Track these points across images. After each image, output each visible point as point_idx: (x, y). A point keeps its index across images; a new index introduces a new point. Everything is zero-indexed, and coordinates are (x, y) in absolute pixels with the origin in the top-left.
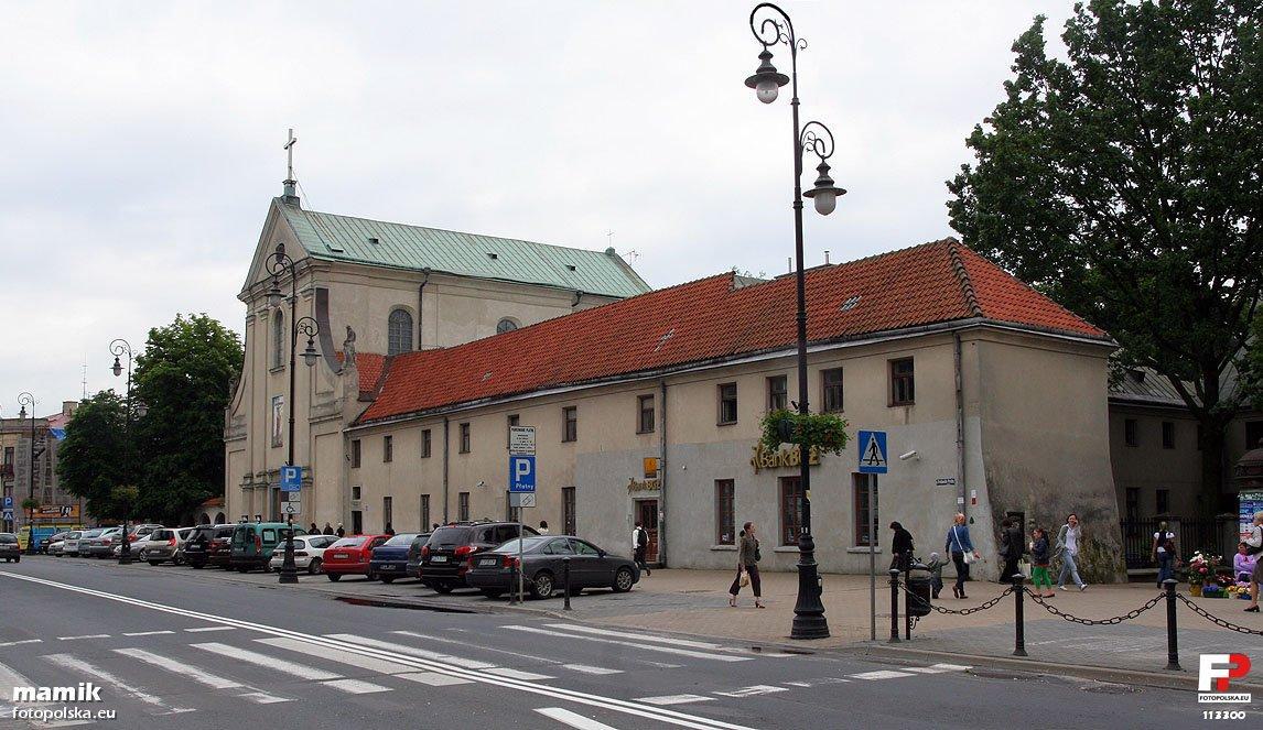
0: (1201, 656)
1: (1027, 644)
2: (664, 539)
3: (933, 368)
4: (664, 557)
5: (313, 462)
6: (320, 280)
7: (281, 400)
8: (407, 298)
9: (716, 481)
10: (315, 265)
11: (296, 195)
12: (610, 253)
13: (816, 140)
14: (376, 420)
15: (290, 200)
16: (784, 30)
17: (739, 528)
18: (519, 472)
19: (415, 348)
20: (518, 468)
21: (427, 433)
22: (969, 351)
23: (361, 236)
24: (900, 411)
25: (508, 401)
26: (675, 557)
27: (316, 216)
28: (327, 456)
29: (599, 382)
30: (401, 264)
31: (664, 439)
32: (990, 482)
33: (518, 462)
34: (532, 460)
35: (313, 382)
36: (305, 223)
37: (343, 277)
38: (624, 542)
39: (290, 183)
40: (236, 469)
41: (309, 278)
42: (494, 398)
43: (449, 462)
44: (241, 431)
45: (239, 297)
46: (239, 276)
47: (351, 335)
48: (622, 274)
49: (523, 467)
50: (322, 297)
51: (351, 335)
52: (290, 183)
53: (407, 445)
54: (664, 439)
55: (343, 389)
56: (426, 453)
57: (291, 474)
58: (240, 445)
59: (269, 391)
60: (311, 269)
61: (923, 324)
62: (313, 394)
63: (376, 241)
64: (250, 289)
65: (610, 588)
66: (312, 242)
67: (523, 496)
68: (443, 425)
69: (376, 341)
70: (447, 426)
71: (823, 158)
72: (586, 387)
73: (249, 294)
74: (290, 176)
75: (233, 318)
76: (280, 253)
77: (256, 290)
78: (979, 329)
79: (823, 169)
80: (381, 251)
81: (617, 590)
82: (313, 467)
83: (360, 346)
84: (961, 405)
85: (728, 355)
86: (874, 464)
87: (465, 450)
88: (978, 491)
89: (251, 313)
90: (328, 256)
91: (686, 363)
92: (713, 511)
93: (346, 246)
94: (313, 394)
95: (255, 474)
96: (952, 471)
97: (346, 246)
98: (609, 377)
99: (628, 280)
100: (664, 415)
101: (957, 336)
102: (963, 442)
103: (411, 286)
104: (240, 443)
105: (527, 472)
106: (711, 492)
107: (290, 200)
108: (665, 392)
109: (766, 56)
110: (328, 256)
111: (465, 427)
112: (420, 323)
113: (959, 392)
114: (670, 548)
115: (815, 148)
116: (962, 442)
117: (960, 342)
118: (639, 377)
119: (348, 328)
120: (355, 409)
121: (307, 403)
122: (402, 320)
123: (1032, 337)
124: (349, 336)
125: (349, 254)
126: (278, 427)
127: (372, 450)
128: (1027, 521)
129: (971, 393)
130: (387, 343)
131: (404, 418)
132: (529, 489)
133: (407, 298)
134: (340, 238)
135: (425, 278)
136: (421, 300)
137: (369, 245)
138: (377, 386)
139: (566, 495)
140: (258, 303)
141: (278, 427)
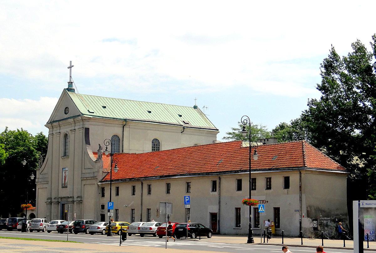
4: (219, 231)
5: (82, 194)
7: (67, 169)
8: (118, 131)
9: (235, 208)
11: (73, 88)
15: (70, 89)
16: (248, 121)
18: (186, 200)
19: (121, 152)
20: (110, 204)
21: (134, 188)
24: (286, 190)
26: (222, 231)
31: (220, 194)
32: (308, 211)
33: (186, 197)
35: (83, 163)
37: (95, 123)
38: (207, 224)
39: (70, 83)
40: (42, 194)
43: (143, 198)
46: (47, 119)
52: (70, 83)
54: (220, 194)
61: (292, 167)
62: (83, 168)
67: (187, 205)
72: (191, 176)
73: (51, 124)
74: (70, 80)
75: (46, 133)
76: (66, 110)
80: (107, 111)
82: (83, 196)
84: (300, 190)
85: (239, 170)
87: (149, 192)
89: (51, 133)
90: (90, 115)
92: (234, 218)
93: (95, 110)
94: (83, 168)
95: (53, 198)
97: (95, 110)
99: (203, 120)
100: (220, 187)
102: (301, 200)
103: (120, 126)
106: (234, 211)
107: (70, 89)
108: (220, 180)
112: (123, 141)
113: (300, 187)
114: (221, 228)
116: (301, 200)
121: (80, 172)
125: (97, 114)
126: (65, 179)
129: (303, 187)
141: (65, 179)
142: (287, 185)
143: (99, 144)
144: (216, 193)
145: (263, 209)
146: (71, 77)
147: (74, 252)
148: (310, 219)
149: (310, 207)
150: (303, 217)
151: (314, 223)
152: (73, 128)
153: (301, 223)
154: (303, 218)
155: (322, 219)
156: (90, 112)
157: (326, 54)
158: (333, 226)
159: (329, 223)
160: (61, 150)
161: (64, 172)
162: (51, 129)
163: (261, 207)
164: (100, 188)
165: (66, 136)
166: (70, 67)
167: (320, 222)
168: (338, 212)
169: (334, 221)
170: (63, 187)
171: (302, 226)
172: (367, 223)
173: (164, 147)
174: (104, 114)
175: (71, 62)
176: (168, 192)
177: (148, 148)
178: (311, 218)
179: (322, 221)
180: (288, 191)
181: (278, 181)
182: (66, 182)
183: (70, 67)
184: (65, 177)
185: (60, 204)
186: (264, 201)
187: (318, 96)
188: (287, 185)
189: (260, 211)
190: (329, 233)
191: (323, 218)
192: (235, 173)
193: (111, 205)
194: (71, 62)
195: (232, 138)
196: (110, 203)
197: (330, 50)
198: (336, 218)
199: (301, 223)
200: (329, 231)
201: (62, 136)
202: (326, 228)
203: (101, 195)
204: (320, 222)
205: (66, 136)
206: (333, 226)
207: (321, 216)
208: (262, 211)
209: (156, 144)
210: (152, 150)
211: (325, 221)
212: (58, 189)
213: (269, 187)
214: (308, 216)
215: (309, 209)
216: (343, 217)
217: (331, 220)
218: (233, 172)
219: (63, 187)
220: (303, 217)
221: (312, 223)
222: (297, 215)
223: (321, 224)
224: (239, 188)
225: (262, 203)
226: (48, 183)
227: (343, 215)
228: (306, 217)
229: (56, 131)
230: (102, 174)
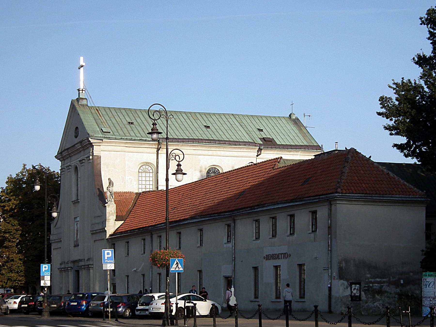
0: (104, 269)
7: (78, 219)
13: (176, 156)
23: (124, 120)
27: (97, 109)
36: (90, 116)
46: (55, 149)
47: (111, 183)
48: (297, 131)
51: (111, 183)
58: (59, 245)
64: (61, 153)
68: (150, 236)
70: (152, 237)
71: (179, 162)
73: (61, 156)
77: (65, 154)
79: (179, 165)
102: (331, 251)
108: (234, 223)
113: (330, 228)
115: (175, 159)
117: (331, 205)
118: (224, 215)
119: (109, 179)
124: (110, 183)
132: (111, 262)
134: (109, 122)
136: (157, 158)
140: (66, 161)
144: (230, 245)
145: (180, 266)
147: (113, 326)
148: (346, 283)
149: (346, 261)
150: (334, 279)
151: (353, 288)
153: (330, 289)
154: (333, 281)
155: (371, 281)
156: (104, 131)
158: (393, 292)
159: (385, 287)
162: (63, 162)
163: (176, 262)
167: (365, 287)
169: (396, 284)
170: (75, 246)
171: (333, 293)
172: (426, 285)
178: (347, 280)
179: (371, 285)
182: (78, 238)
184: (77, 231)
185: (72, 271)
186: (286, 254)
189: (174, 269)
190: (383, 305)
191: (373, 280)
192: (251, 210)
195: (424, 198)
198: (400, 279)
199: (330, 289)
200: (383, 302)
201: (73, 170)
202: (377, 297)
204: (365, 287)
205: (76, 168)
206: (393, 292)
207: (369, 276)
208: (177, 269)
211: (376, 285)
214: (341, 276)
215: (344, 265)
217: (390, 283)
218: (248, 209)
219: (75, 246)
220: (334, 279)
221: (349, 288)
222: (326, 276)
223: (368, 290)
225: (284, 258)
226: (61, 241)
228: (337, 279)
230: (113, 224)
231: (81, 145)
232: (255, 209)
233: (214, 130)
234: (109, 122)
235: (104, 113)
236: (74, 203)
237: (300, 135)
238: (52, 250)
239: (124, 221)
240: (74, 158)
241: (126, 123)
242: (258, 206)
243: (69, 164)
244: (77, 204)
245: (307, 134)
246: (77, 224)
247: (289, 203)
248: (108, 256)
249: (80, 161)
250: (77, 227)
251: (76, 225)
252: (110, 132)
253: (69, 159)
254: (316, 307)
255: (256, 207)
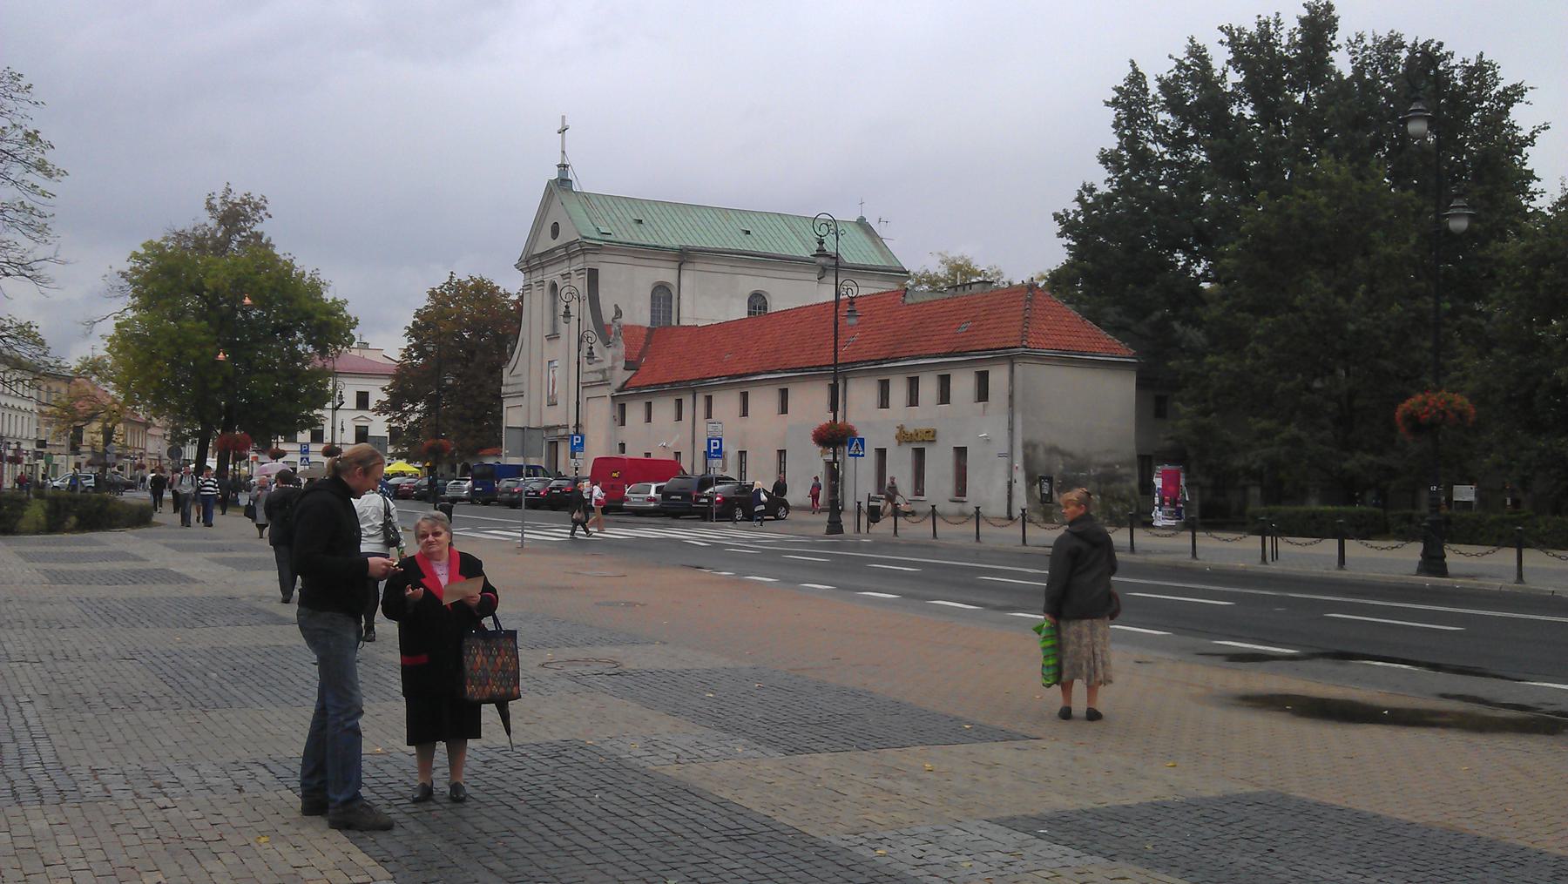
1: (898, 531)
2: (842, 489)
3: (998, 377)
6: (592, 261)
7: (556, 364)
10: (584, 247)
11: (569, 177)
12: (862, 223)
14: (639, 388)
17: (888, 481)
18: (713, 448)
19: (674, 323)
21: (679, 402)
22: (1017, 368)
23: (627, 216)
25: (740, 381)
27: (587, 196)
28: (598, 413)
29: (803, 372)
30: (662, 244)
33: (712, 442)
34: (720, 440)
39: (563, 167)
41: (581, 258)
42: (730, 377)
44: (518, 388)
45: (517, 266)
46: (518, 251)
47: (619, 313)
48: (872, 246)
49: (715, 444)
50: (593, 275)
51: (619, 313)
52: (563, 167)
53: (664, 409)
55: (612, 357)
56: (679, 418)
57: (577, 439)
58: (518, 402)
59: (544, 356)
60: (584, 252)
63: (640, 221)
65: (773, 517)
66: (579, 226)
67: (716, 461)
69: (639, 314)
74: (563, 160)
75: (511, 283)
77: (535, 262)
78: (1023, 356)
81: (777, 518)
83: (625, 320)
84: (1011, 405)
86: (857, 453)
88: (1019, 462)
89: (528, 282)
90: (598, 240)
91: (859, 362)
93: (614, 228)
96: (1006, 450)
97: (614, 228)
98: (809, 368)
101: (1011, 360)
104: (517, 399)
105: (579, 441)
106: (951, 454)
107: (562, 183)
109: (821, 242)
110: (598, 240)
111: (709, 399)
112: (679, 298)
113: (1011, 397)
116: (1011, 429)
119: (616, 306)
120: (621, 376)
122: (663, 296)
123: (1067, 357)
126: (553, 387)
127: (635, 412)
128: (1055, 482)
129: (1018, 397)
130: (649, 315)
131: (661, 389)
133: (666, 274)
134: (607, 218)
135: (684, 257)
137: (634, 225)
138: (640, 357)
139: (741, 457)
140: (534, 274)
141: (553, 387)
142: (983, 394)
143: (616, 306)
146: (564, 152)
152: (565, 271)
157: (1120, 77)
160: (545, 323)
161: (551, 372)
164: (617, 406)
165: (554, 286)
166: (563, 131)
168: (1109, 459)
173: (776, 305)
174: (635, 238)
175: (563, 117)
176: (784, 410)
177: (739, 311)
180: (984, 406)
181: (964, 383)
182: (555, 392)
183: (563, 131)
187: (1101, 180)
188: (983, 394)
193: (579, 441)
194: (563, 117)
196: (575, 437)
197: (1221, 42)
201: (547, 287)
203: (619, 421)
209: (757, 302)
210: (749, 313)
212: (541, 409)
213: (944, 397)
216: (1123, 471)
224: (884, 402)
227: (1122, 464)
229: (537, 276)
231: (566, 251)
232: (882, 364)
233: (757, 238)
234: (607, 218)
235: (597, 203)
236: (548, 339)
237: (875, 251)
238: (504, 408)
239: (634, 372)
240: (549, 270)
241: (630, 220)
242: (888, 360)
243: (540, 278)
244: (553, 341)
245: (885, 249)
246: (553, 371)
247: (941, 357)
248: (715, 448)
249: (562, 275)
250: (554, 376)
251: (551, 372)
252: (610, 234)
253: (541, 271)
254: (978, 508)
255: (884, 361)
